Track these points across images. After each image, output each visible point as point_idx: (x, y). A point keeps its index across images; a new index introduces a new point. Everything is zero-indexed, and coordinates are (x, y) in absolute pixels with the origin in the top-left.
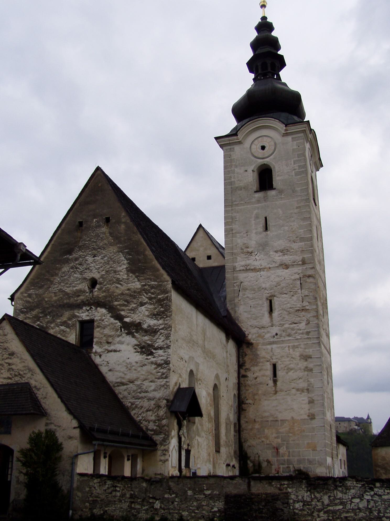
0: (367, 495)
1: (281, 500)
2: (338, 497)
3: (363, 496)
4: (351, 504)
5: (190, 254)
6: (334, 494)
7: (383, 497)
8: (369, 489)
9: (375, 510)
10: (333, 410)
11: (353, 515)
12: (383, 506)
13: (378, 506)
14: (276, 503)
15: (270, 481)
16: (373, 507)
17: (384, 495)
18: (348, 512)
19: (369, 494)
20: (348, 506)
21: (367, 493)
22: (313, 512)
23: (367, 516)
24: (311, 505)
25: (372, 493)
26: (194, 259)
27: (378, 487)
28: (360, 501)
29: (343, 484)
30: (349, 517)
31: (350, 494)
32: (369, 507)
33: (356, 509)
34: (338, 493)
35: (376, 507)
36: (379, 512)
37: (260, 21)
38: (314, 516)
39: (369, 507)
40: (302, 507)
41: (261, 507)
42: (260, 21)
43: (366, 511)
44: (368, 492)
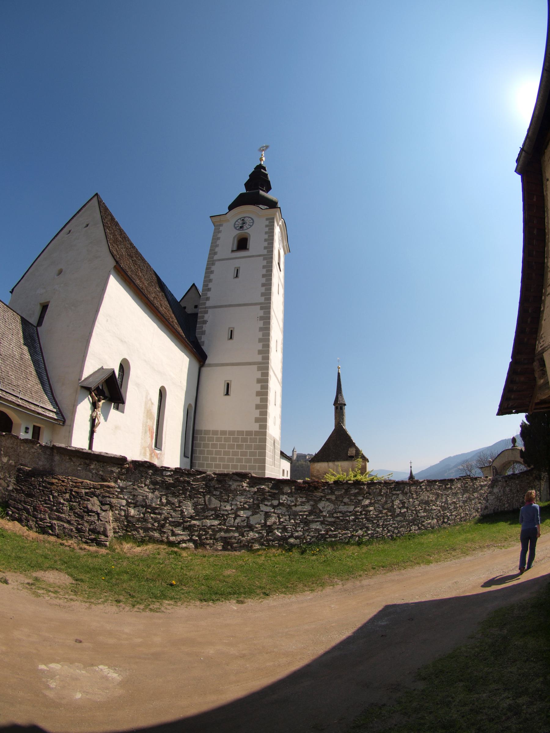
0: (266, 505)
1: (100, 497)
2: (212, 506)
3: (259, 507)
4: (235, 519)
5: (183, 304)
6: (205, 501)
7: (294, 508)
8: (270, 496)
9: (278, 528)
10: (165, 307)
11: (236, 535)
12: (292, 521)
13: (283, 522)
14: (88, 500)
15: (87, 462)
16: (275, 523)
17: (295, 505)
18: (227, 531)
19: (269, 503)
20: (230, 520)
21: (266, 503)
22: (163, 526)
23: (262, 537)
24: (160, 514)
25: (275, 502)
26: (185, 308)
27: (287, 494)
28: (253, 515)
29: (223, 486)
30: (230, 538)
31: (234, 503)
32: (268, 523)
33: (244, 527)
34: (213, 499)
35: (281, 523)
36: (285, 529)
37: (244, 191)
38: (165, 533)
39: (268, 523)
40: (134, 520)
41: (62, 501)
42: (244, 191)
43: (262, 530)
44: (268, 500)
